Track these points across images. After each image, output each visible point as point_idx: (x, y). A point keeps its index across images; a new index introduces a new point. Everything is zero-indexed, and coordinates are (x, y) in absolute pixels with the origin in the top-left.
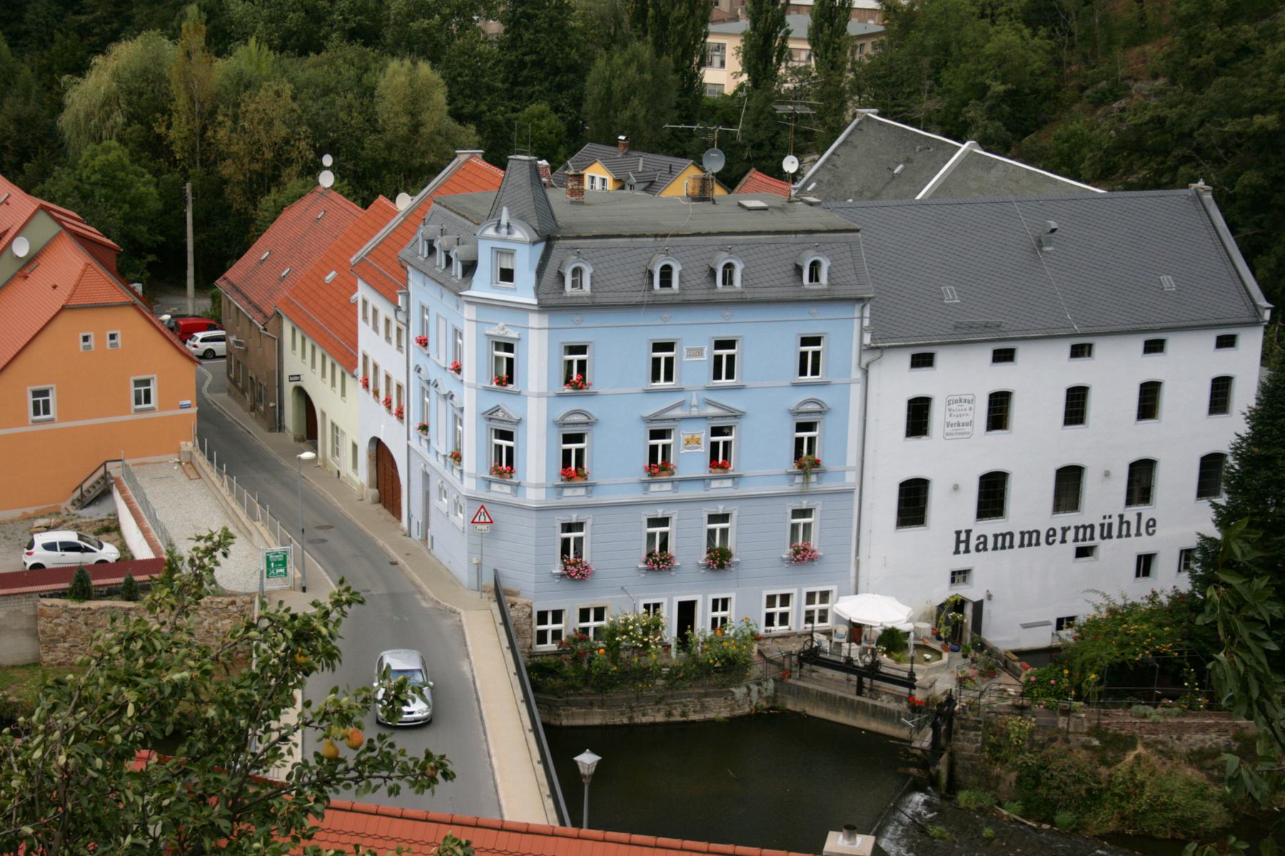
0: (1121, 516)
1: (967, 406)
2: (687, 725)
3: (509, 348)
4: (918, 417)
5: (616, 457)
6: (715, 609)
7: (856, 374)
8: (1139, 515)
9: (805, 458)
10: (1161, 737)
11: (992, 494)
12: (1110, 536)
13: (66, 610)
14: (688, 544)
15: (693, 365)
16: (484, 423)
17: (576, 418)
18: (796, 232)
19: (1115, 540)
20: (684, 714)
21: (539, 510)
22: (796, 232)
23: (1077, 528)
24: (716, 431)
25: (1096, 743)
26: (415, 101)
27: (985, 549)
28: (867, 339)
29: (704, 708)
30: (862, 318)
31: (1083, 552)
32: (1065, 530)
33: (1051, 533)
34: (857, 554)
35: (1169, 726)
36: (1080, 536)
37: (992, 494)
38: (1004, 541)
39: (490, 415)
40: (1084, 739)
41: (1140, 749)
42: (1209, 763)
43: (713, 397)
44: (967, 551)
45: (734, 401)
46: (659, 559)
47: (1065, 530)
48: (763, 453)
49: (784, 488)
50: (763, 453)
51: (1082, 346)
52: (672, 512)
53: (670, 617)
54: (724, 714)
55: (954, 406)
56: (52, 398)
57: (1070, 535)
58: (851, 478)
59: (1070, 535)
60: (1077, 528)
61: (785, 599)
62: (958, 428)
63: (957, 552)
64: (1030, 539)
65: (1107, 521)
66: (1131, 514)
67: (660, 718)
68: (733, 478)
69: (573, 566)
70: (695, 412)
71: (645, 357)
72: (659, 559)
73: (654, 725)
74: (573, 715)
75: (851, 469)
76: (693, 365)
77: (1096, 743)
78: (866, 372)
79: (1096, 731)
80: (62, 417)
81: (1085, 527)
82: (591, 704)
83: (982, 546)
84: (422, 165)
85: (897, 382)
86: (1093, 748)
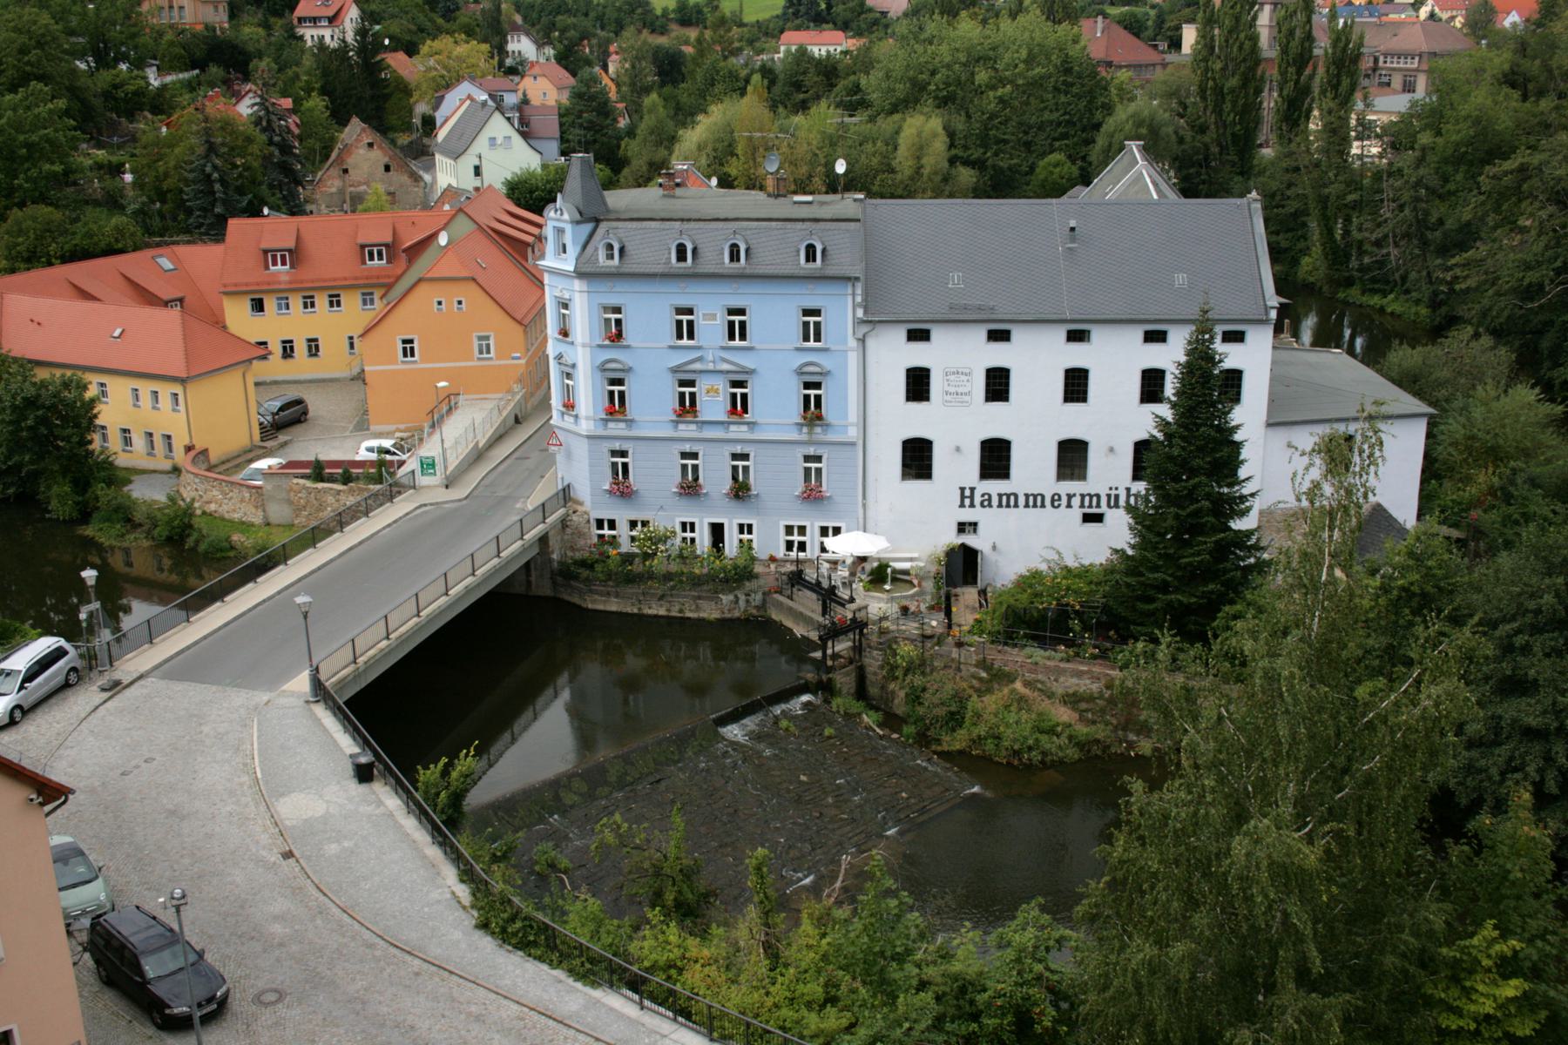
0: (1128, 490)
1: (964, 378)
2: (684, 621)
3: (618, 310)
4: (918, 385)
5: (652, 401)
6: (742, 532)
7: (852, 343)
9: (812, 411)
10: (1040, 677)
11: (995, 458)
13: (304, 487)
14: (716, 477)
15: (711, 328)
16: (599, 374)
17: (613, 366)
18: (803, 220)
20: (681, 611)
21: (588, 437)
22: (803, 220)
23: (1083, 496)
24: (736, 384)
25: (984, 675)
26: (921, 148)
27: (990, 505)
28: (860, 313)
29: (698, 608)
30: (854, 295)
31: (1088, 518)
32: (1070, 497)
33: (1056, 499)
35: (1047, 668)
36: (1087, 503)
37: (995, 458)
38: (1008, 501)
39: (603, 368)
40: (973, 670)
41: (1018, 685)
42: (1083, 706)
44: (972, 505)
45: (746, 361)
46: (691, 488)
48: (776, 405)
49: (794, 436)
53: (703, 539)
54: (715, 615)
55: (952, 377)
56: (416, 345)
57: (1076, 501)
58: (853, 433)
59: (1076, 501)
60: (1083, 496)
61: (802, 530)
62: (958, 397)
63: (962, 505)
64: (1035, 501)
65: (1113, 492)
67: (662, 612)
68: (748, 423)
69: (621, 483)
70: (711, 366)
72: (691, 488)
73: (656, 616)
74: (594, 602)
76: (711, 328)
77: (984, 675)
78: (862, 341)
79: (983, 664)
80: (423, 360)
81: (1091, 496)
82: (608, 594)
83: (987, 502)
85: (893, 355)
86: (980, 679)
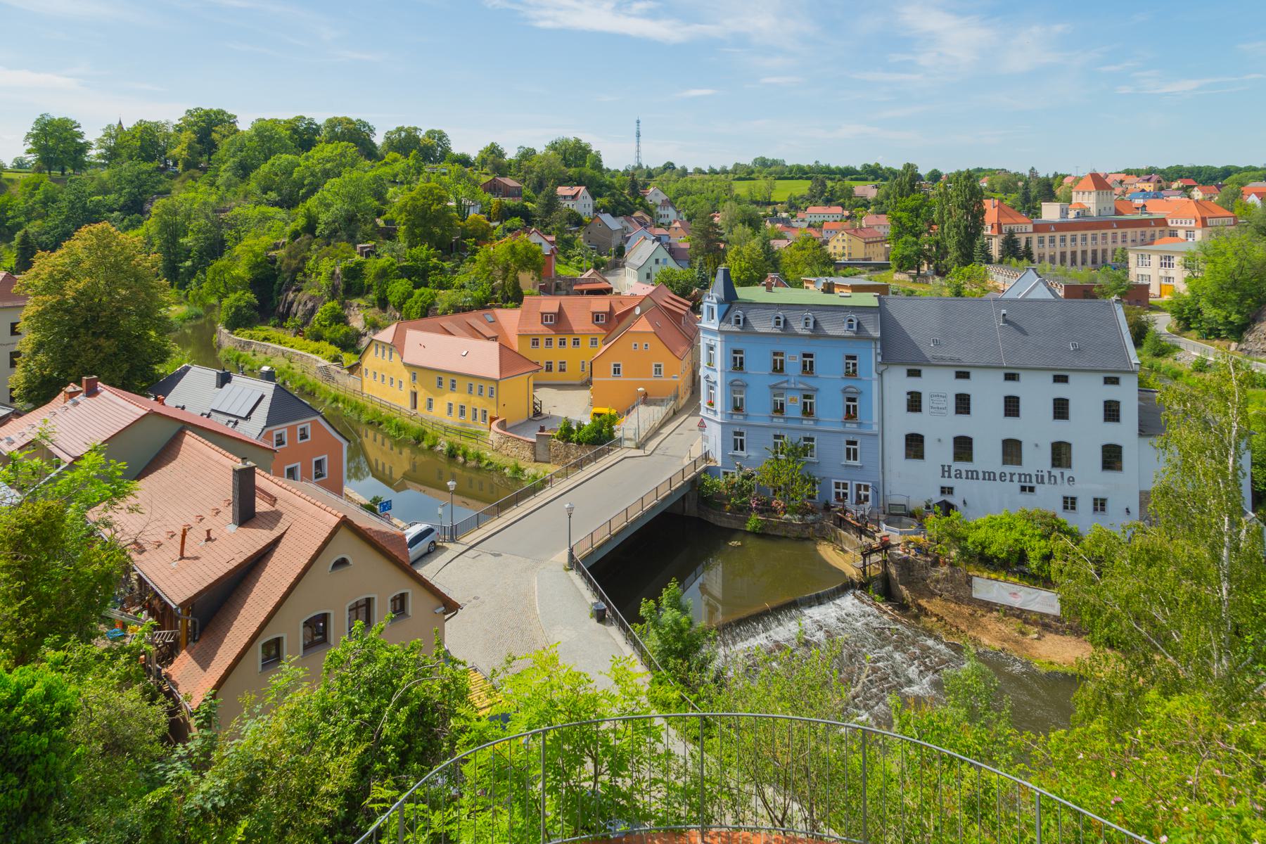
4: (914, 403)
7: (875, 375)
12: (1043, 482)
24: (806, 397)
28: (879, 359)
33: (1002, 476)
38: (972, 475)
48: (830, 408)
50: (830, 408)
57: (1016, 478)
58: (876, 428)
59: (1016, 478)
64: (989, 476)
78: (881, 375)
83: (959, 475)
84: (963, 206)
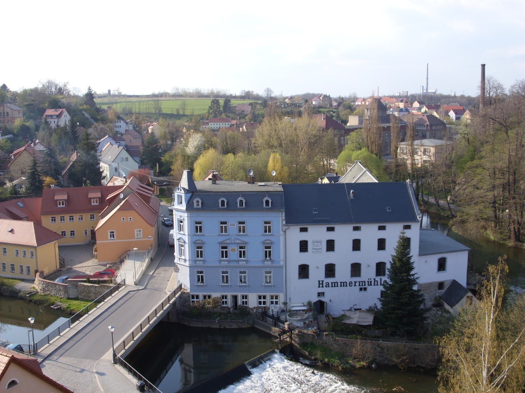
0: (375, 279)
1: (319, 243)
2: (225, 329)
4: (304, 246)
6: (243, 298)
8: (381, 279)
11: (330, 270)
12: (371, 285)
19: (373, 286)
23: (360, 282)
24: (241, 248)
27: (329, 287)
28: (284, 222)
30: (282, 216)
33: (350, 283)
34: (286, 285)
37: (330, 270)
38: (335, 285)
43: (239, 237)
47: (355, 282)
51: (358, 227)
52: (229, 270)
57: (357, 284)
58: (282, 263)
59: (357, 284)
60: (360, 282)
62: (317, 250)
63: (319, 287)
64: (344, 284)
65: (370, 280)
66: (378, 279)
70: (233, 242)
71: (218, 226)
75: (282, 260)
78: (285, 232)
81: (362, 282)
83: (327, 285)
85: (295, 235)
